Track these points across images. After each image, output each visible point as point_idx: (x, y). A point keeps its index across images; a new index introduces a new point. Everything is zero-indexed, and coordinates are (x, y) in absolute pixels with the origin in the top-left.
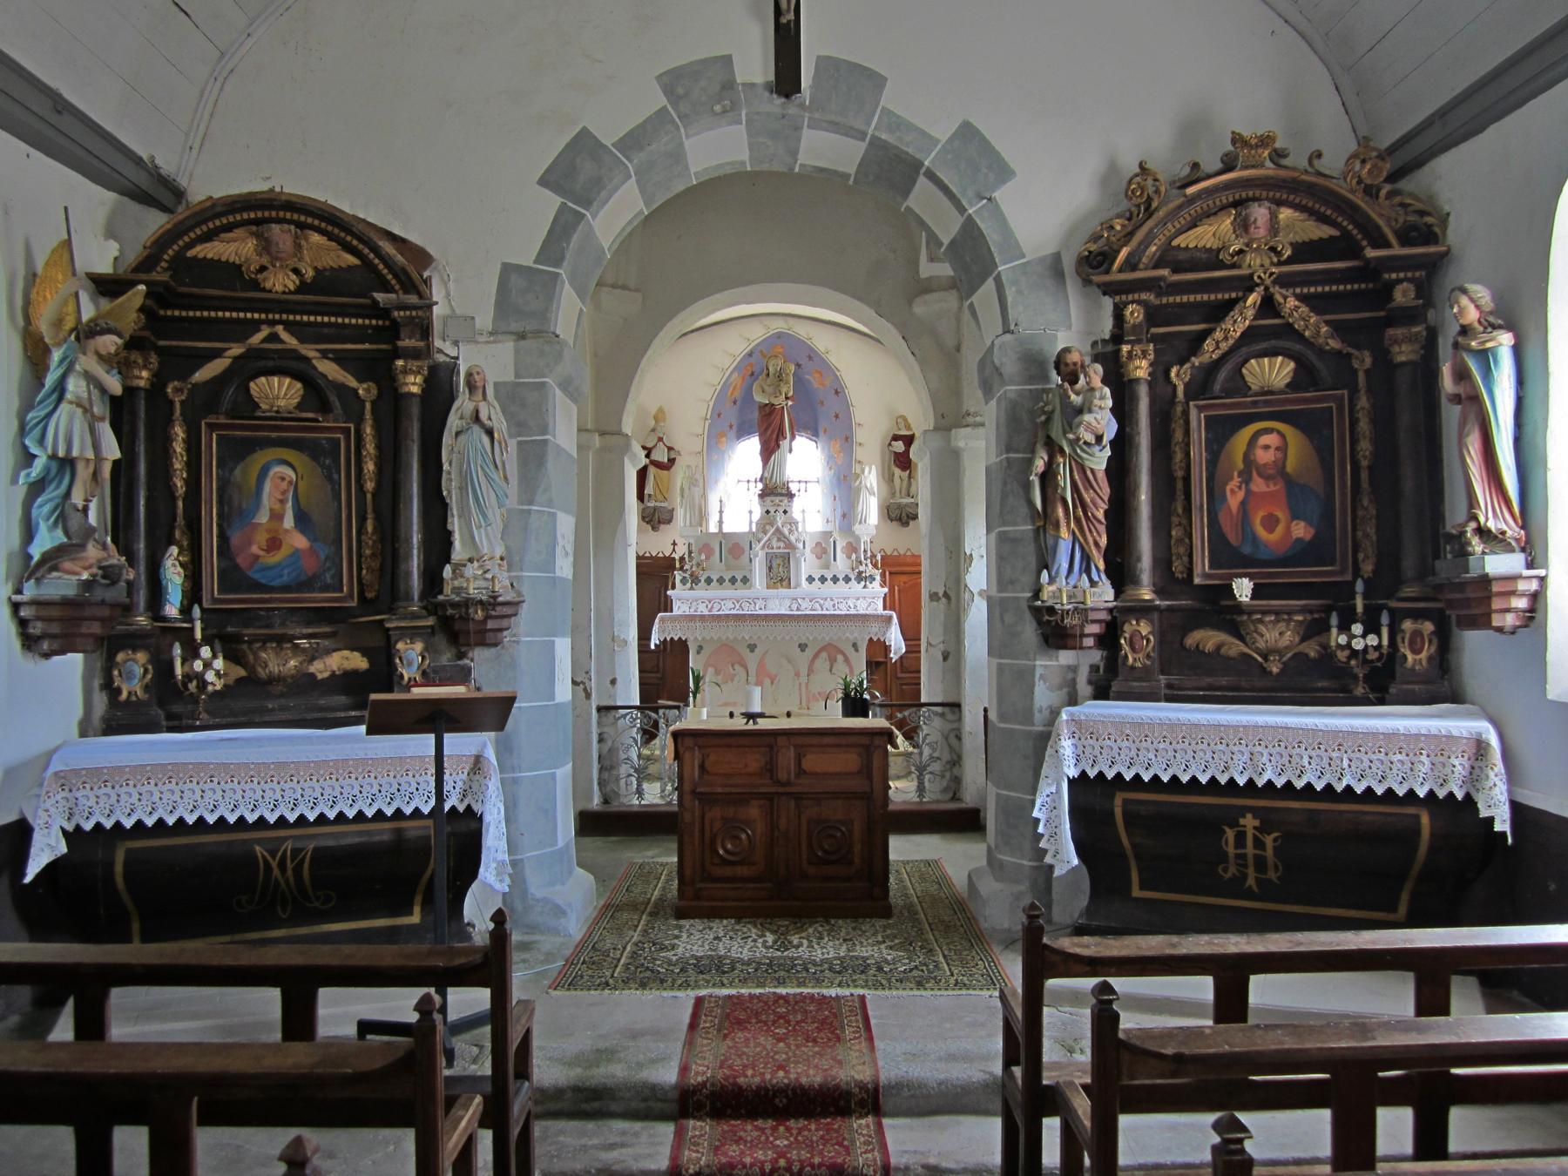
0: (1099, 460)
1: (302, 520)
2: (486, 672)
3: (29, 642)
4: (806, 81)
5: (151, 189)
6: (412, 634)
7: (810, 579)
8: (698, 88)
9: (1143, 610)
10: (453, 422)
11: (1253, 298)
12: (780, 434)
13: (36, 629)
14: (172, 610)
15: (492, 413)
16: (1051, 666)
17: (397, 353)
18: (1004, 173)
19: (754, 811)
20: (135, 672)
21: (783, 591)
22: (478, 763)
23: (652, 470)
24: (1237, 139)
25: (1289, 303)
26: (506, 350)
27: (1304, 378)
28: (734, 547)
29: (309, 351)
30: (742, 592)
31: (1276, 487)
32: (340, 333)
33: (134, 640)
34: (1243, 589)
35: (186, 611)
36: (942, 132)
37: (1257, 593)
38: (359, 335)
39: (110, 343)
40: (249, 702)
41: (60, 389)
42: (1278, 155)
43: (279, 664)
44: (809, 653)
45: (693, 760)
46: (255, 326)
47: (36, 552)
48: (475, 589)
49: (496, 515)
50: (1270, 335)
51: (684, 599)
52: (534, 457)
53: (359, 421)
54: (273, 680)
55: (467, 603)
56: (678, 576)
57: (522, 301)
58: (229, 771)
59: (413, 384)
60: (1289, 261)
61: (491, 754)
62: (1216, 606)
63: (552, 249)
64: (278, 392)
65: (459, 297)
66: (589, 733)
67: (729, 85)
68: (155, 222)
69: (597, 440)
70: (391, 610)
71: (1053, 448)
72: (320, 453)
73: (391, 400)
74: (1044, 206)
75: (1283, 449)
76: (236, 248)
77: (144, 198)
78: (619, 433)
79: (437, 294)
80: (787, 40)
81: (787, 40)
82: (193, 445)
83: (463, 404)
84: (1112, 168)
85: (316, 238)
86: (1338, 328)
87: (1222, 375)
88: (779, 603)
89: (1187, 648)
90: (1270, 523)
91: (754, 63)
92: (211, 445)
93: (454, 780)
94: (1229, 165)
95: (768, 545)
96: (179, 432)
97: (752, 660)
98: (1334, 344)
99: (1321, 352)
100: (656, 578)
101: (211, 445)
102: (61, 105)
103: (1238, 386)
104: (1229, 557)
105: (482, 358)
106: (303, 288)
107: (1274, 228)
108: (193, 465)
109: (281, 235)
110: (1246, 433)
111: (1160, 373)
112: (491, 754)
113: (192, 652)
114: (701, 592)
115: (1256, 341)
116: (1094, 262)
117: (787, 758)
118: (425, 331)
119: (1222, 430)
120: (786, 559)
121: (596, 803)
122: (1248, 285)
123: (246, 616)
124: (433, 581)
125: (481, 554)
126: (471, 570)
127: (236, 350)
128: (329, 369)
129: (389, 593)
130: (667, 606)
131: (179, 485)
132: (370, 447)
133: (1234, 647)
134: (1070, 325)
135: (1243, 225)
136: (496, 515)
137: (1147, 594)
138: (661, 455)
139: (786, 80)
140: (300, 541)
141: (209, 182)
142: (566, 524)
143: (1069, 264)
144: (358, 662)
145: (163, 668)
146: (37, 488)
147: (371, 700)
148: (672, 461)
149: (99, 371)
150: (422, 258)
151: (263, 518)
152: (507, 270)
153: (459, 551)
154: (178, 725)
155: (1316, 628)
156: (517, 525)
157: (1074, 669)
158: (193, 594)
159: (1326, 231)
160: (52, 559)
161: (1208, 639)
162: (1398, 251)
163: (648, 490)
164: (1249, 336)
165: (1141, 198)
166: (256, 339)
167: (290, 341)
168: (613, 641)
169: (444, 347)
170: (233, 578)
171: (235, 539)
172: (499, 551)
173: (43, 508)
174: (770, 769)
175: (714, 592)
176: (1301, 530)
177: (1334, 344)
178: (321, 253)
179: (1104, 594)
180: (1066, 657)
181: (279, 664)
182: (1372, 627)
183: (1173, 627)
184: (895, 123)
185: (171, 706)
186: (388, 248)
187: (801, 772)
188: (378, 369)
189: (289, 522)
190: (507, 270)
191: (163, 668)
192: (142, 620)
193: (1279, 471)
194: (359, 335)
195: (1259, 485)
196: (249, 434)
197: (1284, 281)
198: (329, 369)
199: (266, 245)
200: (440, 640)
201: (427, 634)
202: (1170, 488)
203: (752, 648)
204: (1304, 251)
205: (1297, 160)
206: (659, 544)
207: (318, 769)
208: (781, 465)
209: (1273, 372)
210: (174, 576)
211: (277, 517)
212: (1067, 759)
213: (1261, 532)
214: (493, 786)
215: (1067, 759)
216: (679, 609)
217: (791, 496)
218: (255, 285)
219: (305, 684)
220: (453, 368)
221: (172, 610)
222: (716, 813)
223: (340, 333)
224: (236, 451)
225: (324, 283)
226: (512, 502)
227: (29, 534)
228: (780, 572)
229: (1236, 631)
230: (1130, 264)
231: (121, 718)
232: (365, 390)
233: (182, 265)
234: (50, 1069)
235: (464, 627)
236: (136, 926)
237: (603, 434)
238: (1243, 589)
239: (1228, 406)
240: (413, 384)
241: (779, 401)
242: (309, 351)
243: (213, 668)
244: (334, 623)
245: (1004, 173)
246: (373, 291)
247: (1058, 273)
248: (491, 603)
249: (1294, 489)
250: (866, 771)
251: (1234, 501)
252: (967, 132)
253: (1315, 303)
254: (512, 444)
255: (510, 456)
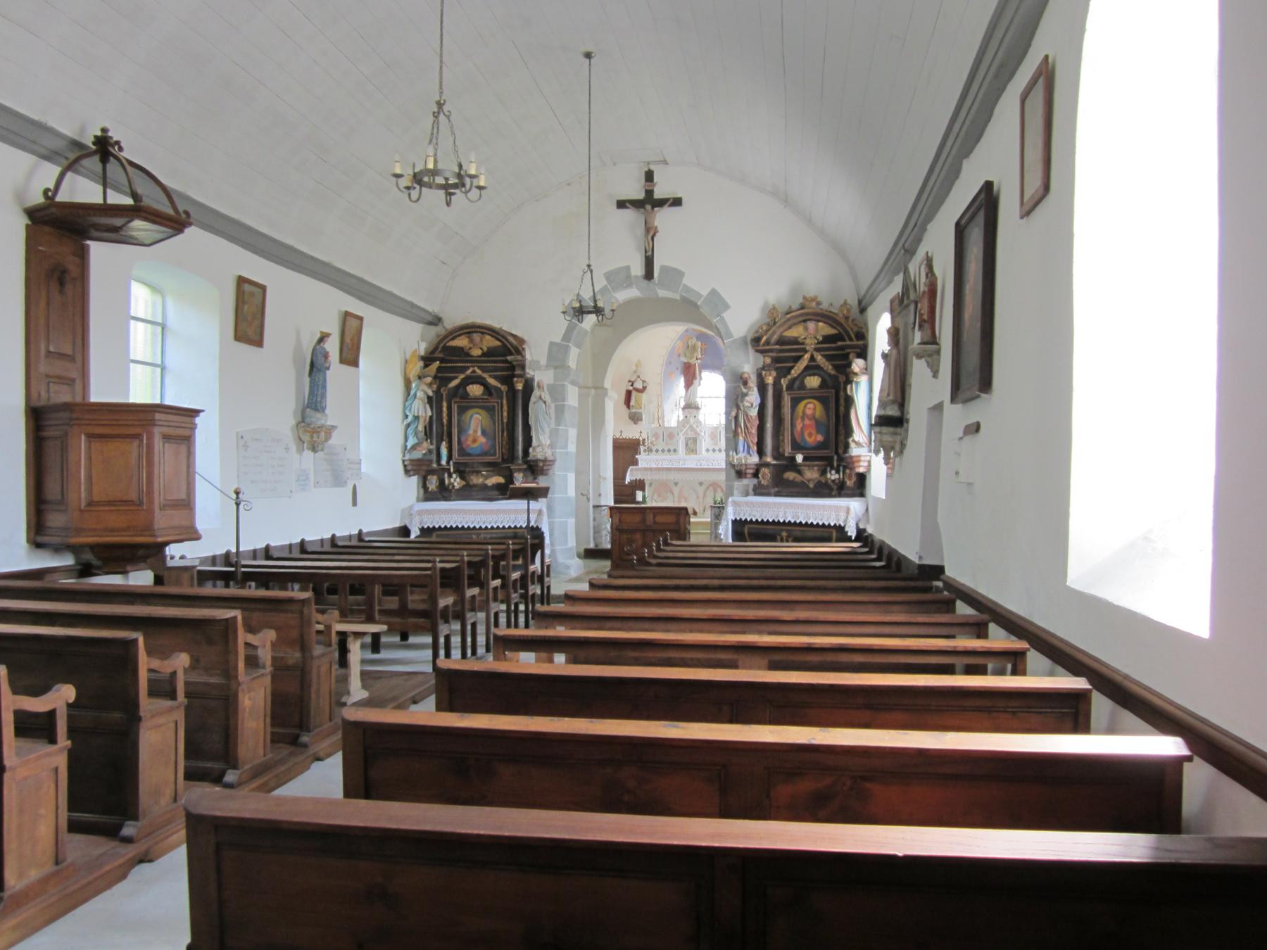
0: (754, 413)
1: (484, 433)
2: (542, 482)
3: (407, 472)
4: (656, 275)
5: (436, 321)
6: (519, 470)
7: (708, 450)
8: (619, 278)
9: (767, 465)
10: (533, 399)
11: (807, 356)
12: (694, 377)
13: (409, 468)
14: (444, 462)
15: (546, 396)
16: (739, 484)
17: (514, 376)
18: (727, 307)
19: (638, 536)
20: (433, 483)
21: (693, 456)
22: (540, 512)
23: (634, 393)
24: (804, 298)
25: (819, 358)
26: (551, 373)
27: (824, 385)
28: (671, 434)
29: (485, 375)
30: (672, 456)
31: (813, 423)
32: (495, 369)
33: (432, 472)
34: (799, 458)
35: (448, 463)
36: (705, 292)
37: (805, 459)
38: (502, 369)
39: (429, 380)
40: (468, 492)
41: (415, 395)
42: (819, 303)
43: (476, 480)
44: (704, 487)
45: (617, 517)
46: (468, 368)
47: (409, 444)
48: (539, 456)
49: (547, 430)
50: (812, 368)
51: (644, 459)
52: (560, 410)
53: (502, 398)
54: (475, 486)
55: (537, 461)
56: (642, 448)
57: (557, 355)
58: (465, 512)
59: (520, 386)
60: (821, 343)
61: (545, 510)
62: (791, 465)
63: (567, 336)
64: (475, 390)
65: (536, 358)
66: (588, 516)
67: (629, 276)
68: (434, 331)
69: (593, 391)
70: (512, 462)
71: (738, 408)
72: (490, 410)
73: (512, 392)
74: (742, 318)
75: (815, 409)
76: (461, 342)
77: (430, 323)
78: (603, 388)
79: (528, 356)
80: (649, 262)
81: (649, 262)
82: (449, 408)
83: (536, 393)
84: (766, 304)
85: (488, 337)
86: (836, 367)
87: (797, 383)
88: (691, 462)
89: (782, 479)
90: (810, 435)
91: (638, 269)
92: (455, 408)
93: (533, 518)
94: (802, 308)
95: (686, 433)
96: (445, 404)
97: (676, 490)
98: (833, 372)
99: (830, 375)
100: (626, 451)
101: (455, 408)
102: (413, 305)
103: (802, 386)
104: (797, 447)
105: (541, 375)
106: (484, 355)
107: (817, 330)
108: (450, 415)
109: (476, 337)
110: (804, 402)
111: (776, 383)
112: (545, 510)
113: (450, 476)
114: (653, 456)
115: (812, 368)
116: (756, 340)
117: (650, 518)
118: (523, 367)
119: (795, 402)
120: (695, 440)
121: (592, 546)
122: (806, 352)
123: (465, 464)
124: (526, 453)
125: (542, 446)
126: (539, 449)
127: (462, 376)
128: (492, 381)
129: (510, 456)
130: (635, 463)
131: (445, 421)
132: (505, 408)
133: (798, 478)
134: (749, 364)
135: (806, 329)
136: (547, 430)
137: (769, 459)
138: (639, 385)
139: (649, 275)
140: (483, 440)
141: (454, 318)
142: (573, 433)
143: (749, 340)
144: (501, 480)
145: (442, 482)
146: (408, 426)
147: (506, 491)
148: (644, 388)
149: (426, 388)
150: (522, 341)
151: (471, 432)
152: (552, 344)
153: (534, 443)
154: (446, 499)
155: (824, 473)
156: (554, 434)
157: (747, 486)
158: (450, 457)
159: (833, 332)
160: (414, 448)
161: (790, 475)
162: (855, 343)
163: (632, 403)
164: (807, 368)
165: (773, 317)
166: (469, 372)
167: (479, 372)
168: (599, 479)
169: (530, 372)
170: (462, 452)
171: (463, 439)
172: (548, 442)
173: (410, 430)
174: (644, 521)
175: (660, 456)
176: (820, 438)
177: (833, 372)
178: (490, 342)
179: (755, 459)
180: (745, 481)
181: (476, 480)
182: (838, 472)
183: (778, 472)
184: (687, 289)
185: (444, 493)
186: (511, 339)
187: (655, 522)
188: (508, 380)
189: (479, 433)
190: (552, 344)
191: (442, 482)
192: (435, 465)
193: (813, 417)
194: (502, 369)
195: (807, 422)
196: (466, 403)
197: (817, 350)
198: (492, 381)
199: (471, 341)
200: (529, 473)
201: (524, 471)
202: (778, 420)
203: (676, 484)
204: (827, 339)
205: (825, 306)
206: (631, 432)
207: (491, 512)
208: (695, 394)
209: (813, 382)
210: (444, 452)
211: (476, 431)
212: (730, 514)
213: (807, 438)
214: (545, 518)
215: (730, 514)
216: (641, 464)
217: (697, 408)
218: (468, 355)
219: (484, 487)
220: (532, 379)
221: (444, 462)
222: (625, 537)
223: (495, 369)
224: (463, 410)
225: (490, 353)
226: (553, 425)
227: (406, 439)
228: (692, 446)
229: (800, 472)
230: (767, 343)
231: (428, 496)
232: (504, 388)
233: (448, 350)
234: (312, 713)
235: (535, 468)
236: (276, 730)
237: (596, 388)
238: (799, 458)
239: (797, 393)
240: (520, 386)
241: (693, 361)
242: (485, 375)
243: (456, 482)
244: (494, 467)
245: (727, 307)
246: (505, 355)
247: (746, 343)
248: (545, 461)
249: (818, 424)
250: (677, 523)
251: (799, 427)
252: (713, 292)
253: (828, 358)
254: (553, 406)
255: (552, 411)
